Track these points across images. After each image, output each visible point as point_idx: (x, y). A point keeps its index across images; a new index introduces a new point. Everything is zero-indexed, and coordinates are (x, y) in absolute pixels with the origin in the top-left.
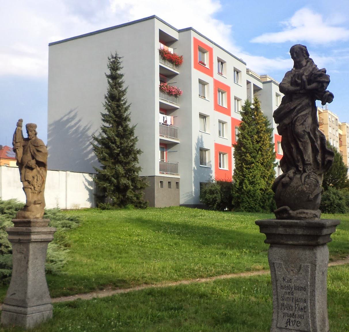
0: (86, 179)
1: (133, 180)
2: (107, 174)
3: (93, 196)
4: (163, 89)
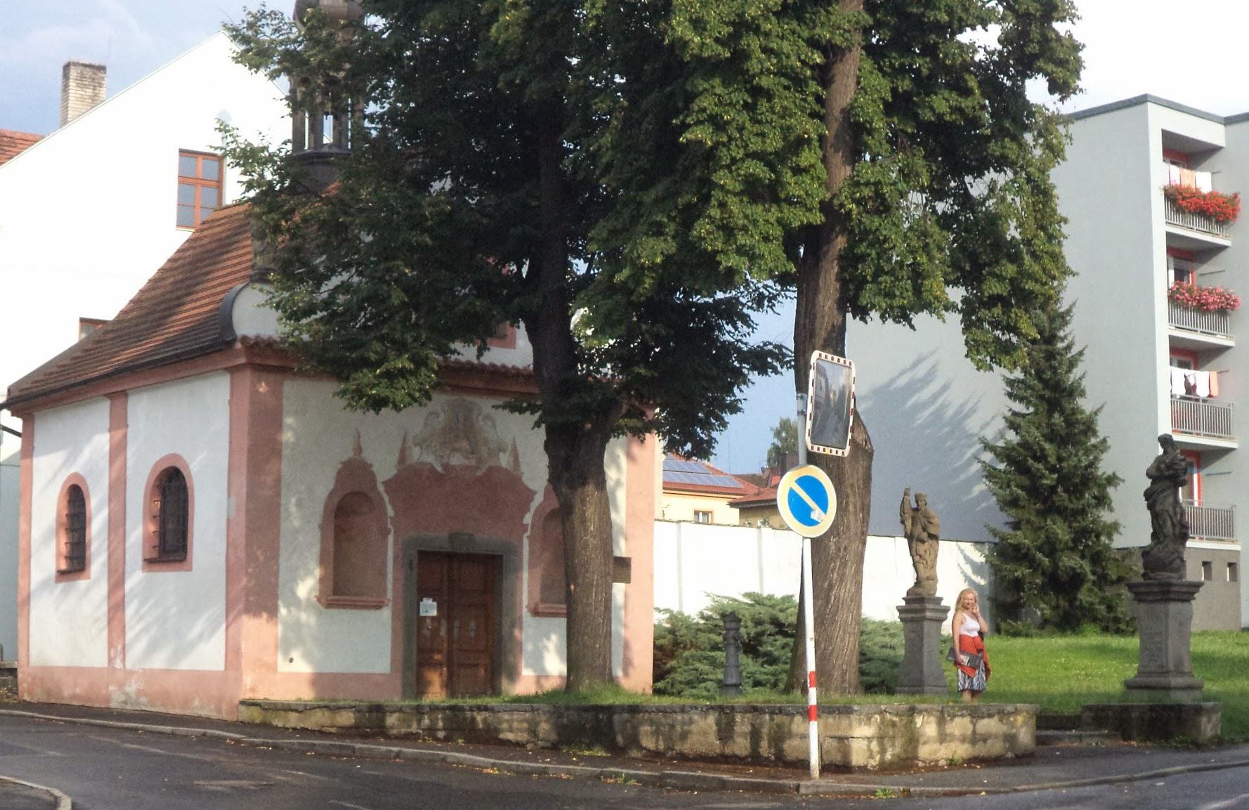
0: (968, 560)
1: (1097, 558)
2: (1024, 544)
3: (987, 604)
4: (1178, 299)
